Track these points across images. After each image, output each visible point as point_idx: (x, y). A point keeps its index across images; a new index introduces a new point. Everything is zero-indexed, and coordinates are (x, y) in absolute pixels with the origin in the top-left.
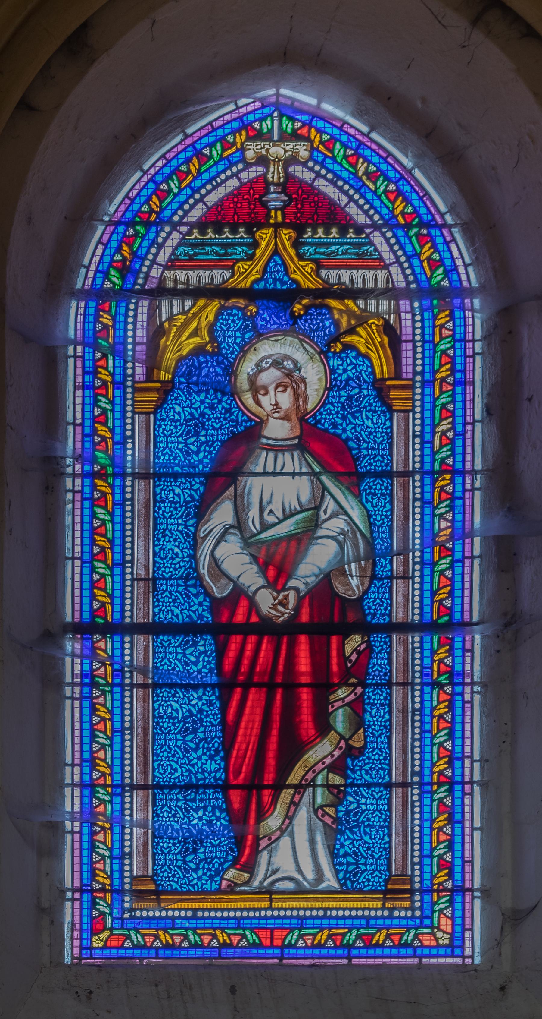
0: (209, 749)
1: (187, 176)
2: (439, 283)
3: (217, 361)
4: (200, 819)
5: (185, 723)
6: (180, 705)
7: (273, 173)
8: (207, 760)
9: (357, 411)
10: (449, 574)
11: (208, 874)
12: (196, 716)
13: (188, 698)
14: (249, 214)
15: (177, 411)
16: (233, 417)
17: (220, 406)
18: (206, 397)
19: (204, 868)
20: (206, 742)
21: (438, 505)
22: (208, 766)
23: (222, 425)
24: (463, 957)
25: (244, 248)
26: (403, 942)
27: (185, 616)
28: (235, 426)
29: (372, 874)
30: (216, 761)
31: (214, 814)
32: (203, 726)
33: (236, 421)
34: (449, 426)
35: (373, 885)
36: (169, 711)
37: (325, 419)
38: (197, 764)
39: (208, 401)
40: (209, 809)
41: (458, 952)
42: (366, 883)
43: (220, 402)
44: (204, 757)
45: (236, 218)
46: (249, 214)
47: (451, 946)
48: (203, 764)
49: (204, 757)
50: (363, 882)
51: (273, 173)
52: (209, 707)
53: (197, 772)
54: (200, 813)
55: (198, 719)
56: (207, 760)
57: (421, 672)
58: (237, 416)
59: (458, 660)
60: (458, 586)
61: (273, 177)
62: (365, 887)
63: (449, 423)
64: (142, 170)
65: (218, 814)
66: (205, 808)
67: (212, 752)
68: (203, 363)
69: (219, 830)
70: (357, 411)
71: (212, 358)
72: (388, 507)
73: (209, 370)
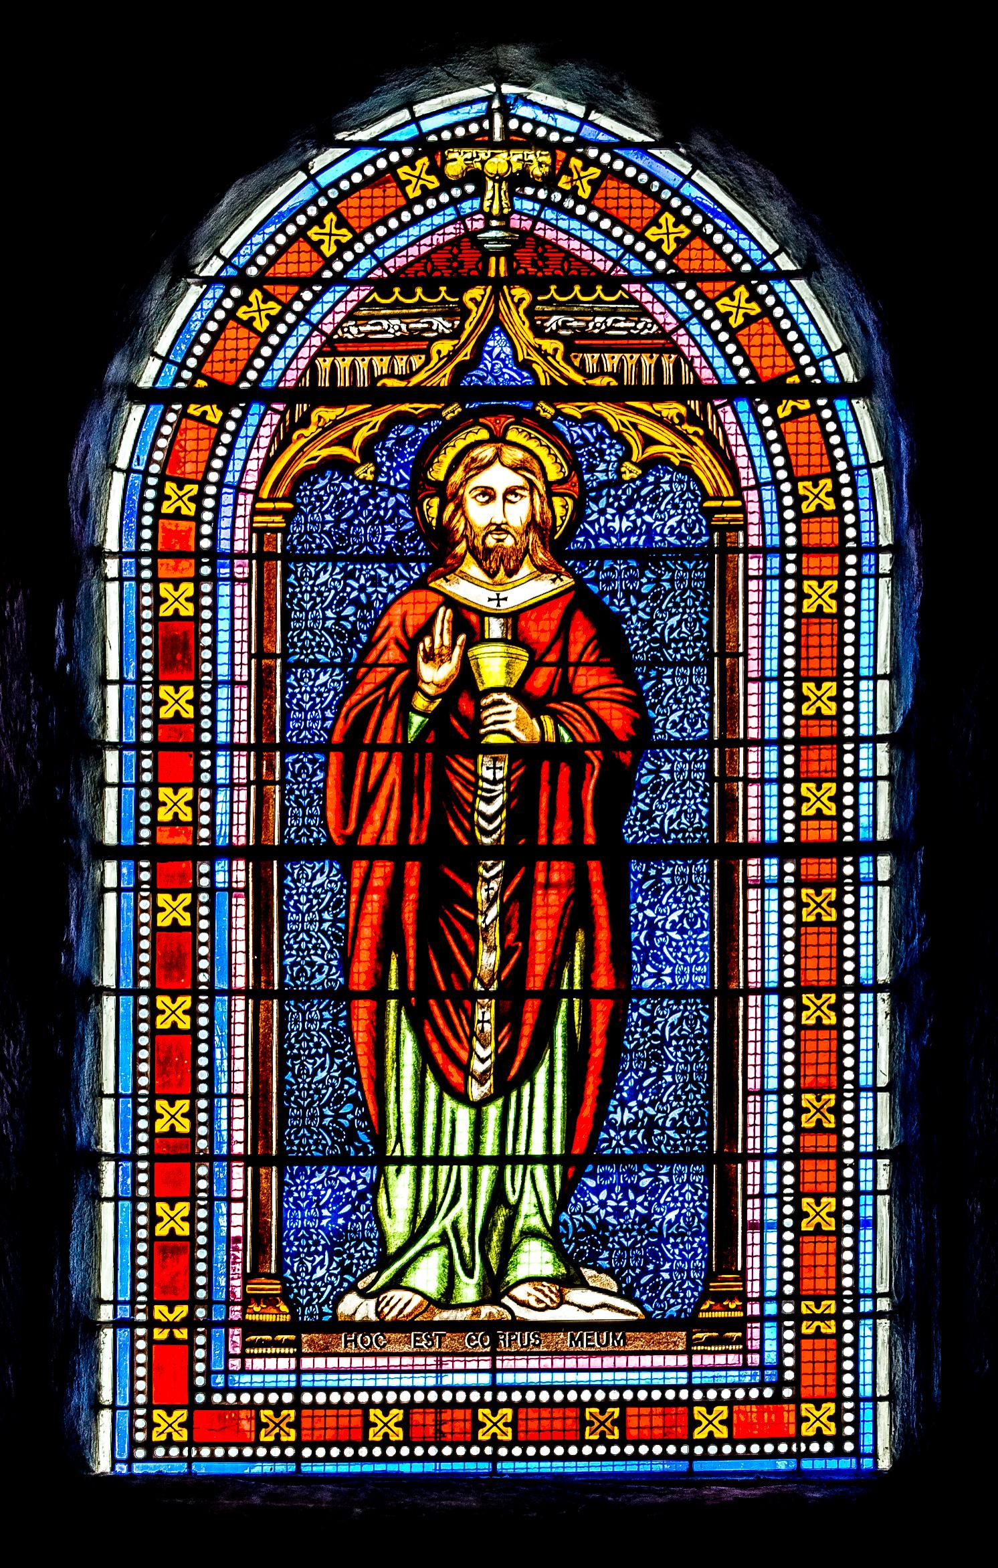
3: (626, 1138)
4: (603, 1204)
5: (578, 1245)
8: (613, 515)
9: (582, 1235)
13: (584, 1203)
17: (632, 1212)
18: (609, 1197)
22: (616, 525)
23: (636, 1242)
24: (857, 1454)
28: (659, 649)
30: (630, 1109)
33: (661, 639)
38: (598, 520)
39: (611, 1203)
40: (618, 1188)
43: (632, 1204)
44: (610, 511)
48: (607, 521)
49: (610, 511)
51: (493, 198)
52: (617, 1217)
53: (599, 535)
54: (603, 1195)
56: (613, 515)
58: (662, 633)
61: (491, 207)
65: (631, 1196)
66: (611, 1189)
69: (634, 1223)
70: (582, 1235)
71: (618, 1133)
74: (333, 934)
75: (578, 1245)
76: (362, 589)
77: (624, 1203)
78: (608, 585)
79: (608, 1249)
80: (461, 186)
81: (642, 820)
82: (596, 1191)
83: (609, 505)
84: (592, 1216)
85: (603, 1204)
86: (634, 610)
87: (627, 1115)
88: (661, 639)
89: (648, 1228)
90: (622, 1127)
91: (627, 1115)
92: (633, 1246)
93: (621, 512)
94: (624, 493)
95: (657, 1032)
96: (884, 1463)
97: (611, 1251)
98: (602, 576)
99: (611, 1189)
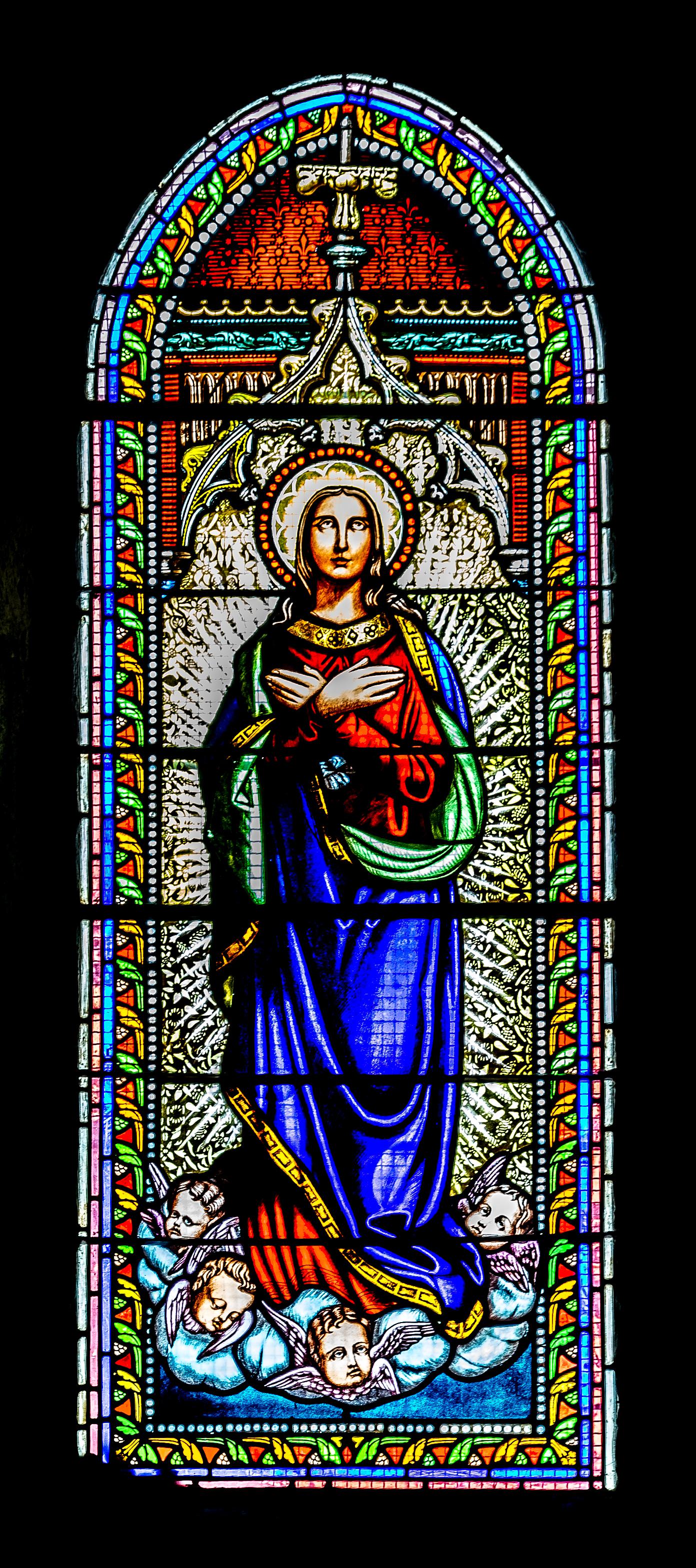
1: (134, 1173)
2: (557, 398)
6: (519, 1013)
7: (342, 215)
10: (572, 1028)
14: (299, 276)
15: (524, 1162)
18: (171, 995)
21: (555, 963)
25: (284, 334)
26: (497, 1459)
34: (571, 1339)
41: (586, 1473)
45: (279, 280)
46: (299, 276)
47: (578, 1466)
57: (532, 550)
59: (584, 800)
60: (584, 859)
63: (570, 1380)
64: (84, 716)
73: (170, 1135)
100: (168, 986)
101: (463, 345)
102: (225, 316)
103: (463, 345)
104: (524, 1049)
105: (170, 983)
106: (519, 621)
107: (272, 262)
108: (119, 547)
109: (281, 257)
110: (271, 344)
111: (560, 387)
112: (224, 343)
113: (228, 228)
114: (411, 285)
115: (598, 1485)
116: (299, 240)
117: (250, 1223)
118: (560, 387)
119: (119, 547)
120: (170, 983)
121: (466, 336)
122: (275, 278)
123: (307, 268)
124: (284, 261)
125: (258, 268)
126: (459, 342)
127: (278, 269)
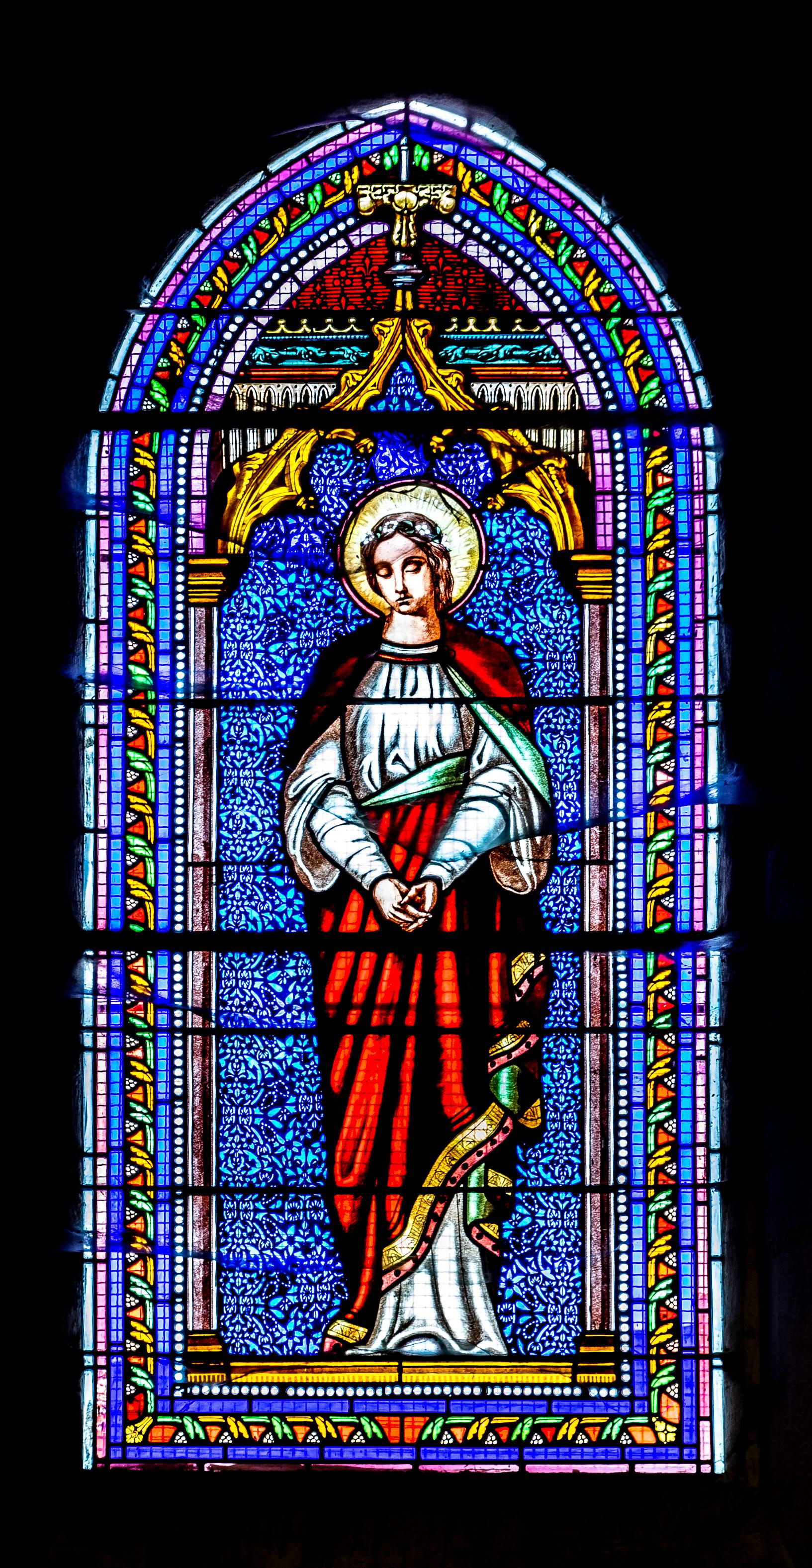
0: (305, 1321)
4: (291, 587)
5: (267, 1090)
11: (302, 1001)
12: (283, 1078)
15: (251, 917)
16: (339, 611)
17: (319, 594)
18: (298, 581)
19: (295, 992)
20: (299, 1120)
22: (302, 1158)
25: (356, 348)
27: (268, 605)
29: (555, 1329)
30: (314, 1150)
31: (312, 1233)
32: (294, 1094)
33: (344, 616)
35: (557, 1347)
36: (245, 732)
37: (320, 606)
40: (304, 1225)
42: (547, 1344)
46: (363, 296)
50: (259, 845)
53: (286, 1167)
55: (287, 1083)
62: (545, 1349)
65: (317, 1232)
66: (298, 1224)
67: (310, 1326)
68: (292, 526)
72: (576, 751)
74: (267, 886)
75: (267, 1090)
76: (319, 587)
77: (311, 1239)
78: (294, 1215)
79: (296, 1284)
80: (184, 487)
81: (326, 606)
82: (285, 1226)
83: (297, 1328)
84: (281, 1252)
85: (290, 903)
86: (319, 1241)
87: (311, 1157)
88: (344, 616)
89: (333, 611)
90: (306, 1167)
91: (311, 1157)
92: (319, 628)
93: (308, 1334)
94: (310, 1126)
95: (339, 611)
96: (720, 1468)
97: (297, 1096)
98: (287, 1207)
99: (298, 1224)
100: (299, 906)
101: (506, 357)
102: (305, 333)
103: (506, 357)
104: (544, 657)
105: (297, 908)
106: (546, 1209)
107: (337, 283)
108: (130, 605)
109: (346, 278)
110: (342, 357)
111: (663, 887)
112: (299, 357)
113: (343, 262)
114: (346, 306)
115: (705, 1469)
116: (363, 262)
117: (419, 962)
118: (663, 887)
119: (130, 605)
120: (297, 908)
121: (509, 347)
122: (339, 299)
123: (371, 288)
124: (348, 282)
125: (324, 289)
126: (501, 355)
127: (342, 290)
